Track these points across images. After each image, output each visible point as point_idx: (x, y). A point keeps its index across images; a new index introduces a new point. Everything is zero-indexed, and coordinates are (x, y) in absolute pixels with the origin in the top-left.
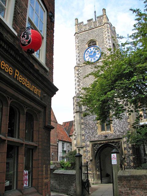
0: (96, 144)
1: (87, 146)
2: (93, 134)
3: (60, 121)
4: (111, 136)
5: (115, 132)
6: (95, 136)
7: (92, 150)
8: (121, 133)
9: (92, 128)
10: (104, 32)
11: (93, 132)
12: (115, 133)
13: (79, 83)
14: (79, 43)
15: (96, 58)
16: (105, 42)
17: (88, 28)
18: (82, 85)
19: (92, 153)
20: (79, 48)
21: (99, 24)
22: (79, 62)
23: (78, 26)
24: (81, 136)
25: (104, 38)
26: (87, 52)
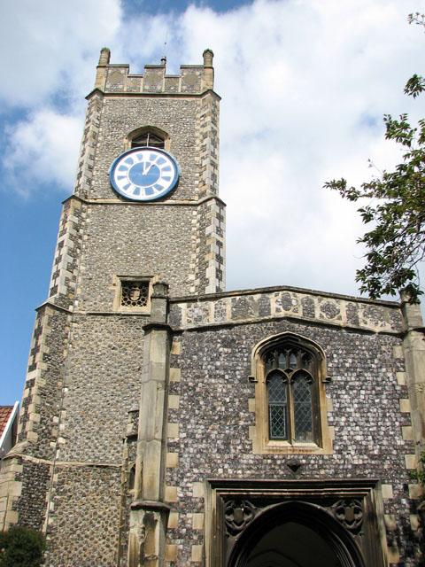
0: (238, 500)
1: (188, 505)
2: (227, 444)
3: (215, 292)
4: (321, 467)
5: (339, 452)
6: (235, 461)
7: (214, 532)
8: (372, 457)
9: (226, 419)
10: (198, 116)
11: (228, 438)
12: (343, 458)
13: (74, 260)
14: (98, 126)
15: (154, 189)
16: (198, 149)
17: (144, 90)
18: (82, 268)
19: (214, 542)
20: (98, 142)
21: (184, 87)
22: (87, 188)
23: (110, 71)
24: (163, 449)
25: (197, 134)
26: (126, 161)
